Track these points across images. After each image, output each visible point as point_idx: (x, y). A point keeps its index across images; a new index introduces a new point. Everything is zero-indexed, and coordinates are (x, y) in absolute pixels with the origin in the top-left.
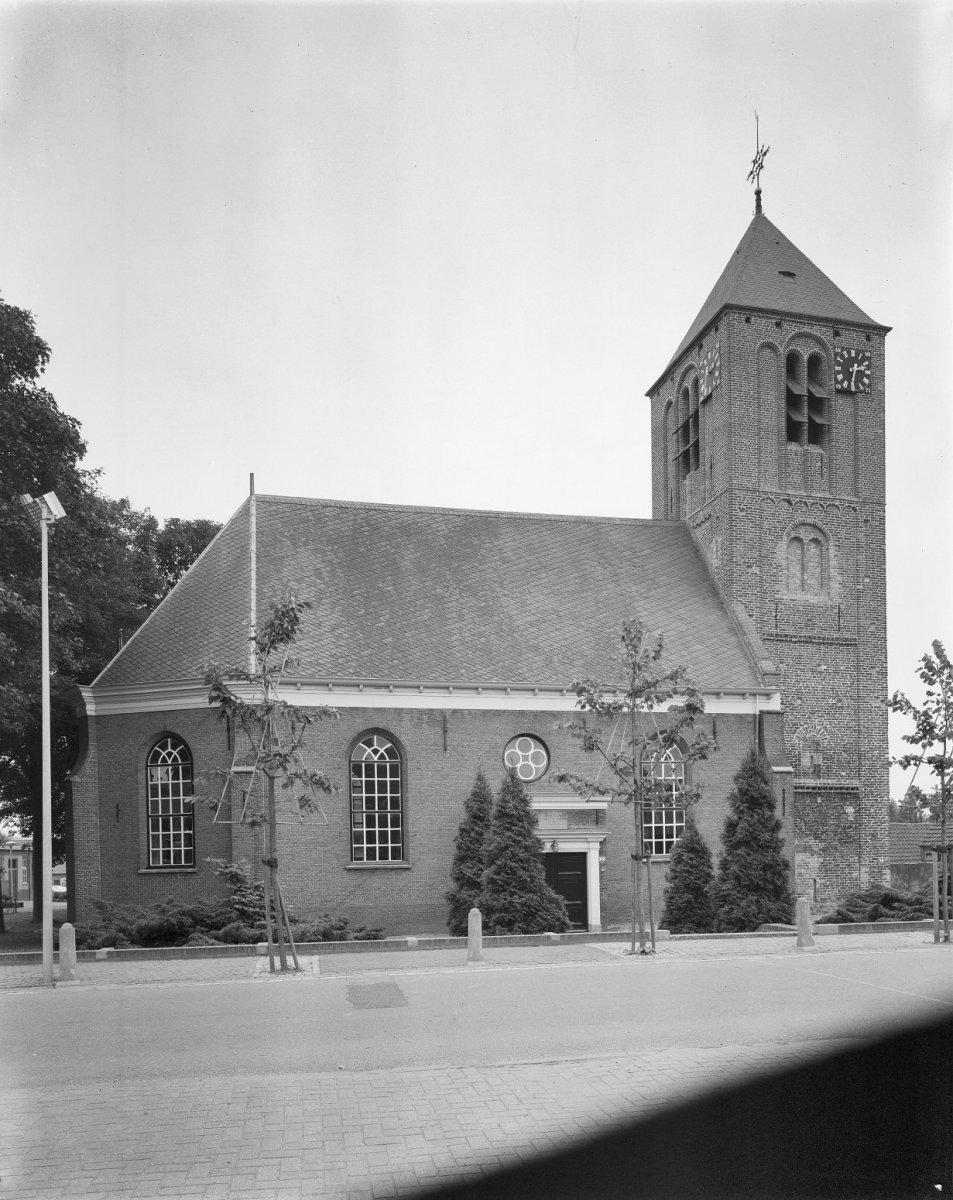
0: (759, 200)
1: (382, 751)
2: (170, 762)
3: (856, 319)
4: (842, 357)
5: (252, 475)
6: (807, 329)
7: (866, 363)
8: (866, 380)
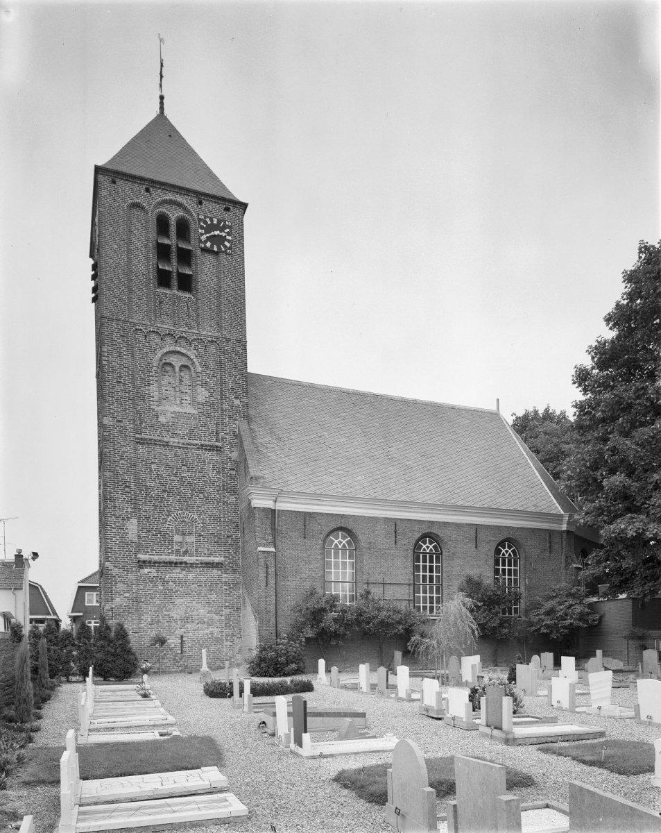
0: (162, 103)
1: (344, 542)
2: (340, 547)
3: (227, 197)
4: (205, 222)
5: (498, 400)
6: (179, 198)
7: (227, 230)
8: (227, 244)
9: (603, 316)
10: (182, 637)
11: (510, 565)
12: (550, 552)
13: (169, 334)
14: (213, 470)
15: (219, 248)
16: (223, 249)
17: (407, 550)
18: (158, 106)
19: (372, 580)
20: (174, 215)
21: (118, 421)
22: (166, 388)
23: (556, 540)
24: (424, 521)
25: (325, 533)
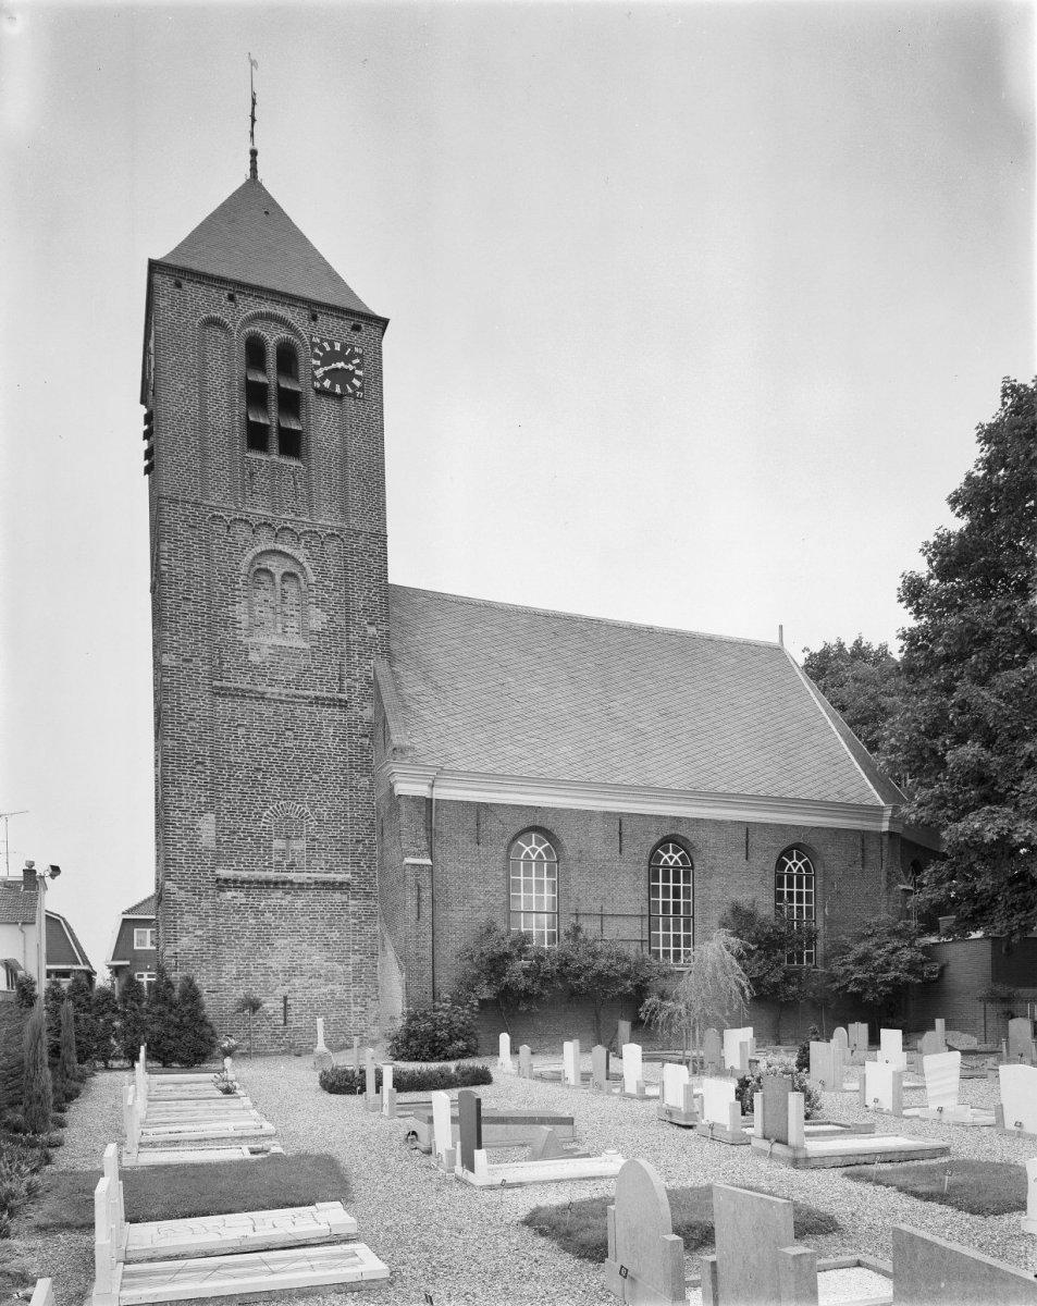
0: (254, 162)
2: (534, 858)
3: (357, 309)
4: (322, 349)
5: (781, 627)
6: (281, 311)
7: (356, 361)
8: (356, 383)
9: (947, 496)
10: (286, 998)
11: (800, 885)
12: (863, 866)
13: (265, 523)
14: (335, 736)
15: (343, 388)
16: (350, 391)
17: (638, 863)
18: (249, 166)
19: (583, 909)
20: (273, 337)
21: (184, 660)
22: (260, 609)
23: (873, 846)
24: (665, 817)
25: (510, 836)
